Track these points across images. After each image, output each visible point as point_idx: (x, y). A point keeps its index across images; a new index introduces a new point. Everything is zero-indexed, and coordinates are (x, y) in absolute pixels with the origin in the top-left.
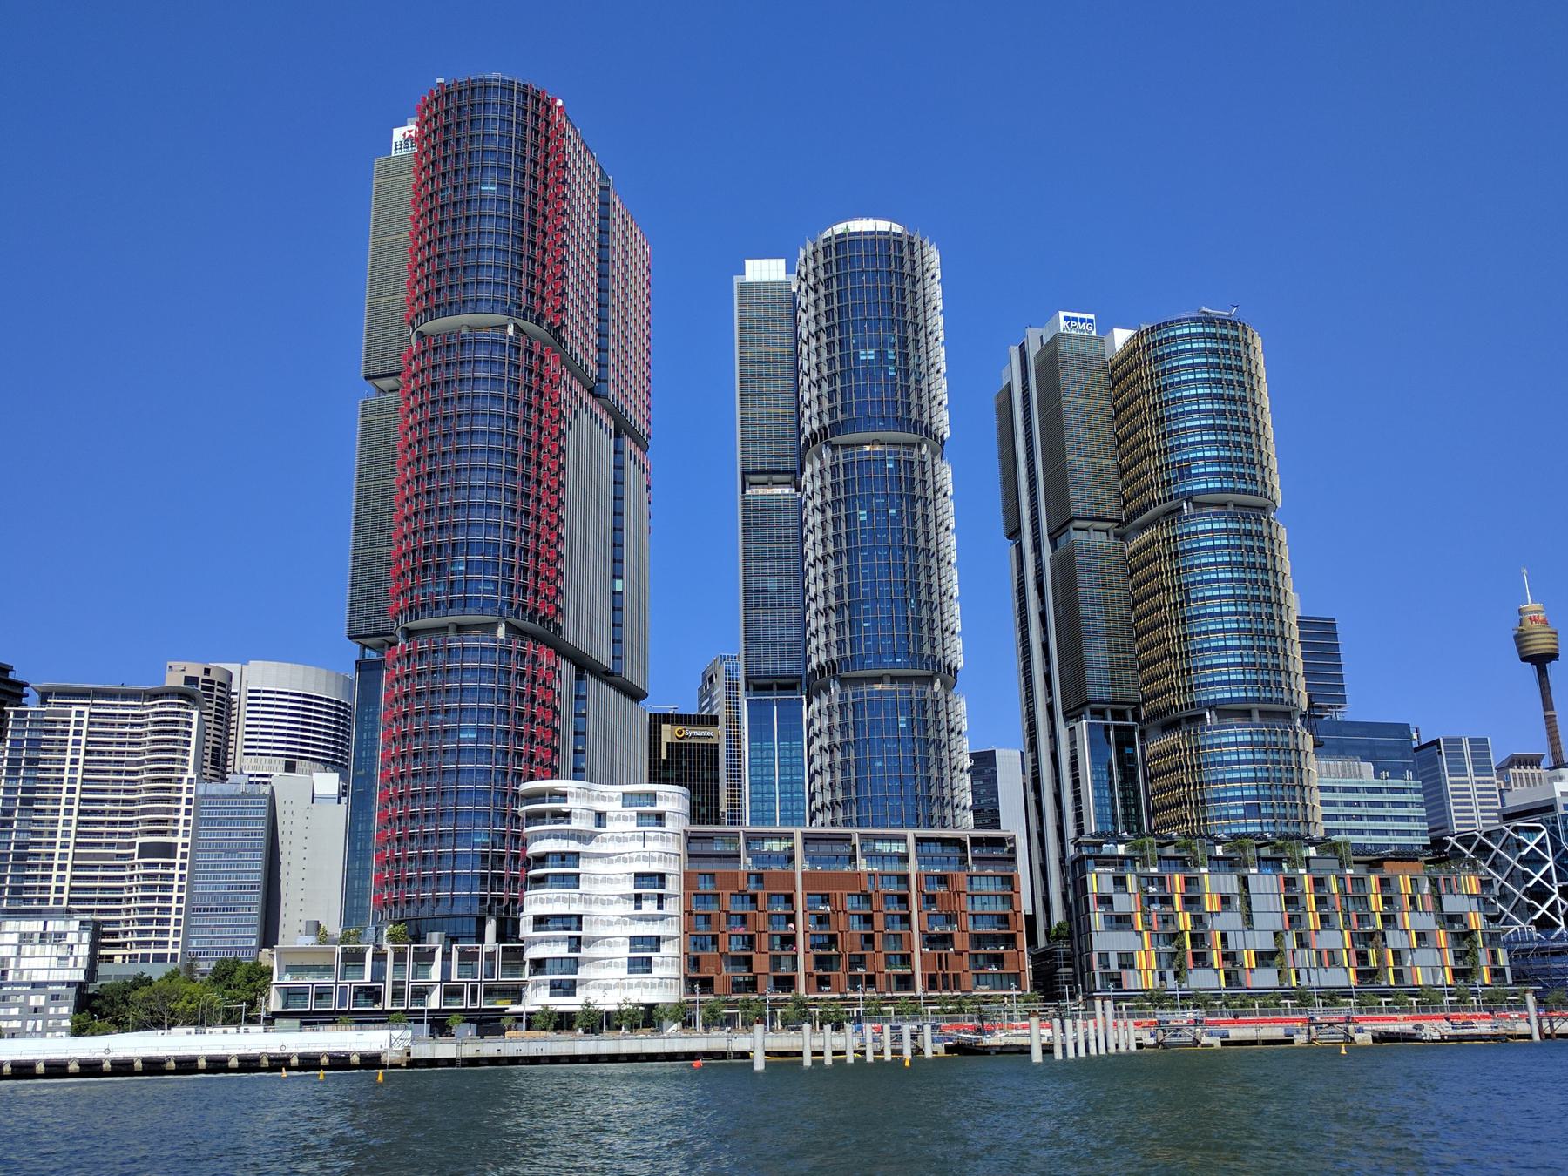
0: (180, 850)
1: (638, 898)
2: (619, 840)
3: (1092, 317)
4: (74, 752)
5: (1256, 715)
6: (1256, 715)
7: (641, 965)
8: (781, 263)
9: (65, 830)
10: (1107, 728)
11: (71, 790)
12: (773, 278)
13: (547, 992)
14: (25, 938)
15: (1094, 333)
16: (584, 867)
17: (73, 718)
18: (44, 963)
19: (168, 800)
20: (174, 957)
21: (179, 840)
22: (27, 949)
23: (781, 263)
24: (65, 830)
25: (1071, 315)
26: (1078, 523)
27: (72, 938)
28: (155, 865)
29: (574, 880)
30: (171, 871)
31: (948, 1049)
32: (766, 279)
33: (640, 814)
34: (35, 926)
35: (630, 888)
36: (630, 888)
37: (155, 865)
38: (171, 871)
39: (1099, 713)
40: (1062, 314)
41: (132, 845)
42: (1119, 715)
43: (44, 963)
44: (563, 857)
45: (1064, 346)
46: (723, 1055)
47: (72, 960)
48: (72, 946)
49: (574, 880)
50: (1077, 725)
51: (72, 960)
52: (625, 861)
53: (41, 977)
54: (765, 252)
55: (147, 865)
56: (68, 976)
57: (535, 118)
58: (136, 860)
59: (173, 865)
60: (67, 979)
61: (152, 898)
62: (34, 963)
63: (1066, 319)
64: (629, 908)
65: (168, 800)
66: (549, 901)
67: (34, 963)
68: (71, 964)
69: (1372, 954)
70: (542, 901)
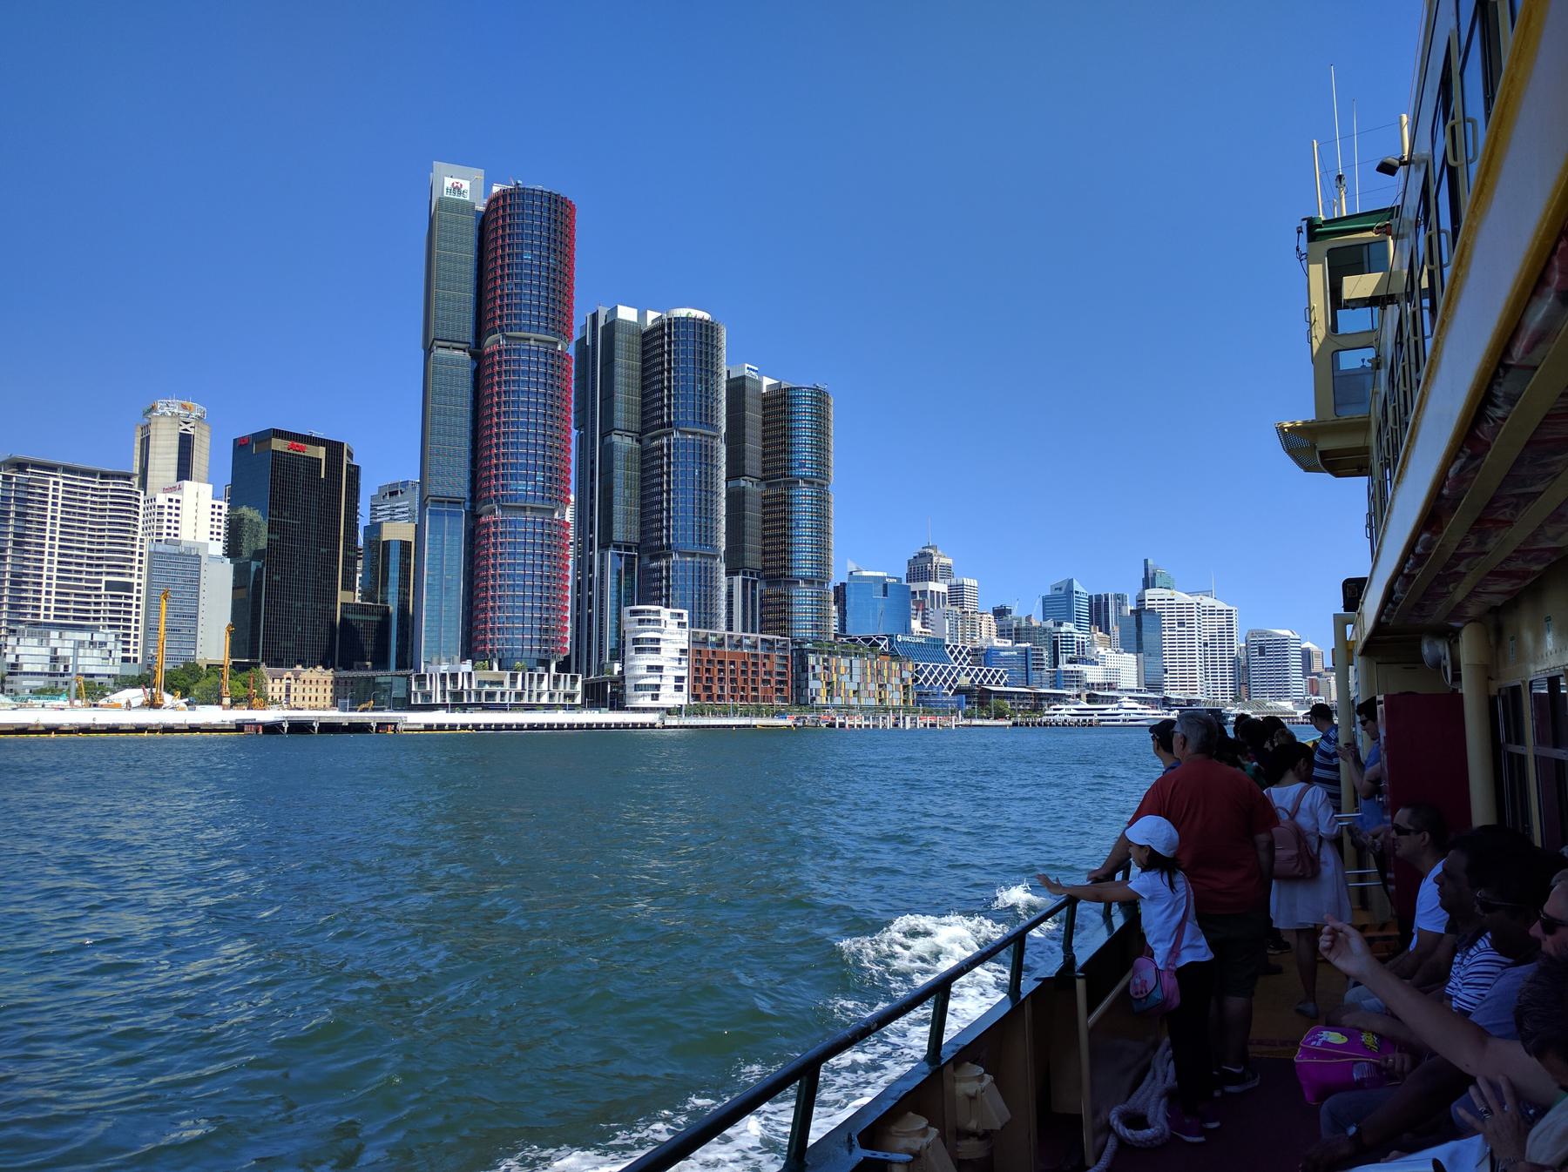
4: (54, 513)
7: (679, 688)
9: (50, 568)
11: (52, 539)
14: (81, 644)
15: (1267, 745)
17: (51, 486)
18: (95, 661)
19: (125, 552)
21: (135, 580)
22: (81, 652)
24: (50, 568)
27: (110, 646)
29: (658, 650)
32: (576, 264)
34: (86, 636)
35: (677, 655)
36: (677, 655)
39: (618, 547)
41: (99, 581)
42: (628, 548)
43: (95, 661)
45: (748, 384)
49: (658, 650)
53: (92, 670)
54: (461, 158)
56: (108, 671)
62: (88, 661)
64: (676, 664)
65: (125, 552)
67: (88, 661)
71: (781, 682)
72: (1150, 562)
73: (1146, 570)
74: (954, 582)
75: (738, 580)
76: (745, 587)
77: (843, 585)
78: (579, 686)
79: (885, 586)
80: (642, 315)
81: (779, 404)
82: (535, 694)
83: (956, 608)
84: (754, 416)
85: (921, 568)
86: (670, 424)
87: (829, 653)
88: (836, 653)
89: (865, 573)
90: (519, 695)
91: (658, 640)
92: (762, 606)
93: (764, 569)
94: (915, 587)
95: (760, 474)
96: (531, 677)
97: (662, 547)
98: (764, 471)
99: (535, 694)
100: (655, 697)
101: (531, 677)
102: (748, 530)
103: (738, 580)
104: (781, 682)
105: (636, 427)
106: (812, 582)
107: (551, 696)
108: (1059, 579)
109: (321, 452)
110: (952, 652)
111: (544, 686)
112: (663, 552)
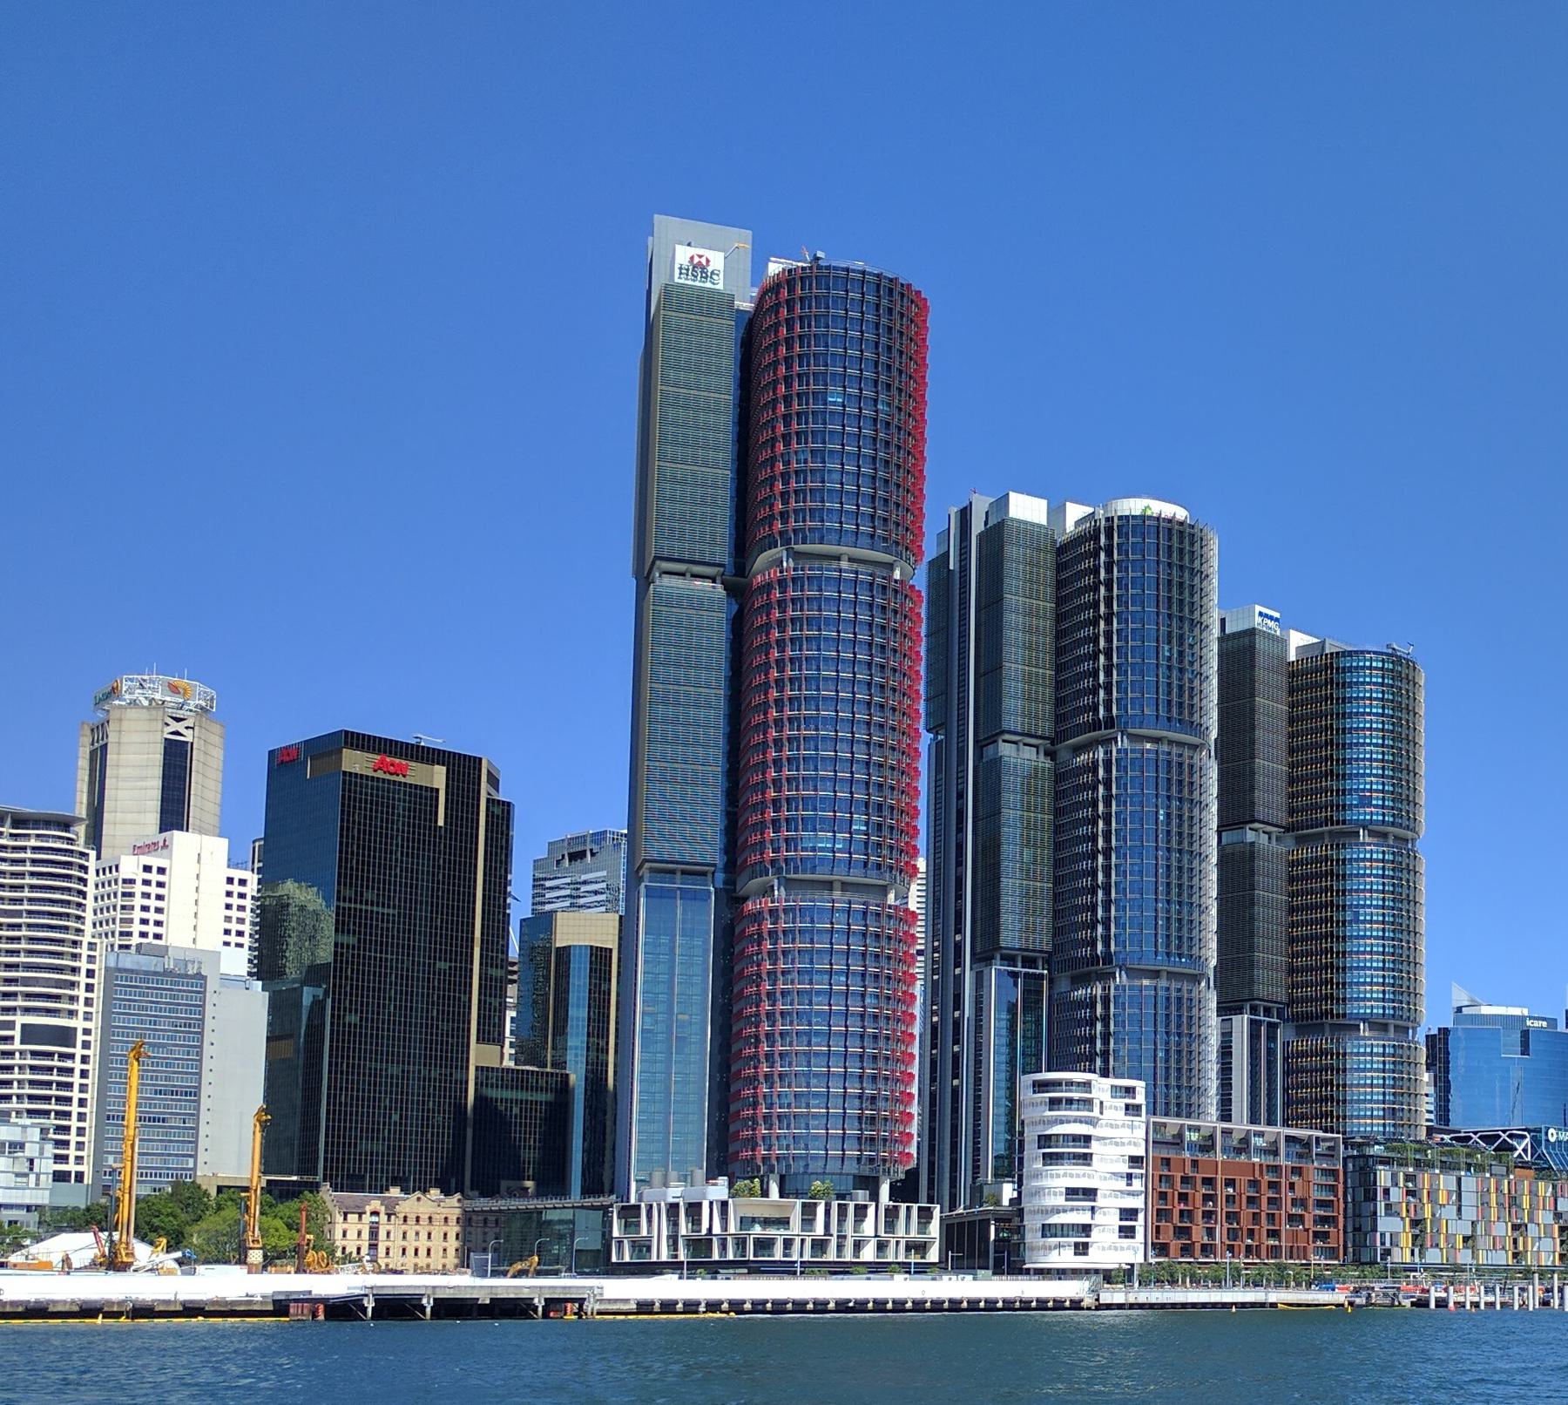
0: (80, 1038)
1: (1130, 1176)
2: (1112, 1126)
3: (1277, 615)
5: (1392, 1029)
6: (1392, 1029)
8: (1042, 505)
10: (1014, 975)
12: (1036, 521)
13: (1072, 1251)
16: (1095, 1147)
19: (59, 969)
20: (80, 1177)
21: (78, 1023)
23: (1042, 505)
25: (1265, 611)
26: (1007, 737)
28: (50, 1055)
29: (1086, 1159)
30: (68, 1064)
31: (1413, 1304)
33: (1127, 1107)
36: (1124, 1168)
37: (50, 1055)
38: (68, 1064)
39: (1009, 959)
40: (1258, 608)
44: (1076, 1139)
45: (1260, 644)
46: (1262, 1305)
47: (32, 1177)
48: (31, 1161)
49: (1086, 1159)
50: (986, 971)
51: (32, 1177)
52: (1117, 1144)
55: (34, 1054)
56: (28, 1198)
57: (895, 311)
58: (17, 1045)
59: (72, 1057)
60: (27, 1201)
61: (47, 1099)
63: (1261, 614)
65: (59, 969)
66: (1078, 1176)
68: (32, 1185)
69: (1521, 1240)
70: (1071, 1176)
75: (1241, 1023)
76: (1254, 1037)
77: (1445, 1032)
78: (934, 1229)
79: (1525, 1034)
80: (1056, 512)
81: (1320, 682)
82: (849, 1243)
84: (1271, 705)
89: (1486, 1010)
90: (820, 1246)
91: (1087, 1139)
92: (1286, 1073)
93: (1292, 1002)
96: (843, 1210)
97: (1094, 959)
99: (849, 1243)
100: (1081, 1249)
101: (843, 1210)
103: (1241, 1023)
105: (1046, 727)
106: (1384, 1027)
107: (881, 1247)
109: (438, 777)
111: (868, 1227)
112: (1096, 968)
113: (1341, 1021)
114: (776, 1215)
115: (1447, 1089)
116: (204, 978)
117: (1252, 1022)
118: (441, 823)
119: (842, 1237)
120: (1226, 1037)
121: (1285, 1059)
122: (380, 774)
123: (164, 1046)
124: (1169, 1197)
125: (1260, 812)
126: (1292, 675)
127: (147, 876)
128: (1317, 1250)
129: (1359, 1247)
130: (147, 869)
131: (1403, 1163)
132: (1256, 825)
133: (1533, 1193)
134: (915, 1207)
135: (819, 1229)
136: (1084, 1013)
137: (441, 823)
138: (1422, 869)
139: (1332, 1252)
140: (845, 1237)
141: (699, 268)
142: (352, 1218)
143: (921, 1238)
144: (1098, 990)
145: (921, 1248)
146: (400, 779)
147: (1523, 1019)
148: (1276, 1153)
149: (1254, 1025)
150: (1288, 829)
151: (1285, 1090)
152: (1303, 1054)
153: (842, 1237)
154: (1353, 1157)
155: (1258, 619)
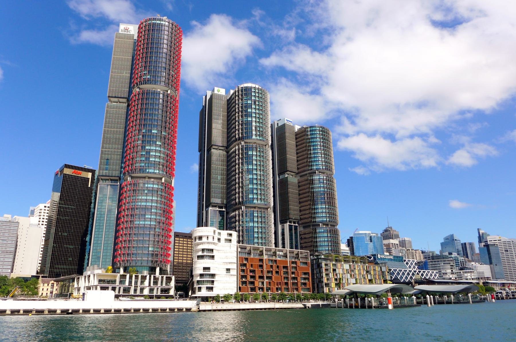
26: (214, 147)
52: (225, 252)
71: (305, 279)
72: (481, 232)
73: (479, 233)
74: (401, 240)
75: (287, 226)
76: (290, 229)
77: (352, 238)
78: (173, 284)
79: (371, 237)
80: (227, 92)
81: (304, 136)
82: (139, 289)
83: (404, 248)
84: (291, 143)
85: (387, 234)
86: (239, 139)
87: (336, 261)
88: (340, 261)
89: (361, 232)
90: (162, 291)
91: (212, 250)
92: (301, 239)
93: (301, 219)
94: (386, 242)
95: (296, 171)
96: (137, 277)
97: (236, 204)
98: (298, 169)
99: (139, 289)
100: (210, 289)
101: (137, 277)
102: (290, 198)
103: (287, 226)
104: (305, 279)
105: (225, 145)
106: (327, 225)
107: (151, 290)
108: (447, 234)
109: (90, 175)
110: (407, 264)
111: (146, 283)
112: (237, 207)
113: (315, 224)
114: (109, 279)
115: (353, 249)
116: (19, 223)
117: (289, 225)
118: (89, 186)
119: (136, 287)
120: (283, 230)
121: (300, 235)
122: (74, 174)
123: (6, 240)
124: (245, 271)
125: (289, 169)
126: (296, 135)
127: (45, 208)
128: (302, 289)
129: (317, 286)
130: (45, 207)
131: (331, 260)
132: (288, 173)
133: (374, 270)
134: (165, 276)
135: (127, 283)
136: (233, 220)
137: (89, 186)
138: (335, 181)
139: (309, 290)
140: (137, 287)
141: (126, 30)
142: (46, 285)
143: (167, 287)
144: (237, 212)
145: (167, 291)
146: (79, 175)
147: (369, 234)
148: (286, 257)
149: (290, 226)
150: (297, 174)
151: (301, 244)
152: (305, 234)
153: (136, 287)
154: (315, 259)
155: (286, 121)
